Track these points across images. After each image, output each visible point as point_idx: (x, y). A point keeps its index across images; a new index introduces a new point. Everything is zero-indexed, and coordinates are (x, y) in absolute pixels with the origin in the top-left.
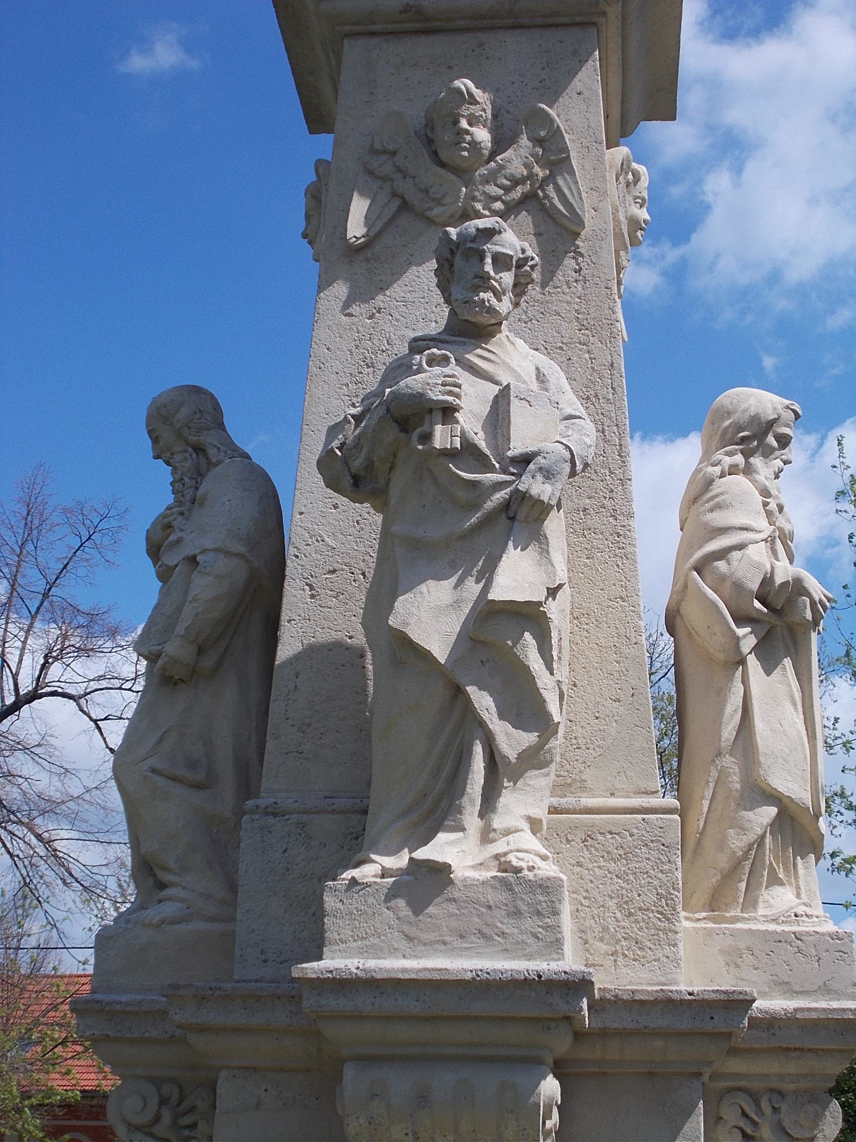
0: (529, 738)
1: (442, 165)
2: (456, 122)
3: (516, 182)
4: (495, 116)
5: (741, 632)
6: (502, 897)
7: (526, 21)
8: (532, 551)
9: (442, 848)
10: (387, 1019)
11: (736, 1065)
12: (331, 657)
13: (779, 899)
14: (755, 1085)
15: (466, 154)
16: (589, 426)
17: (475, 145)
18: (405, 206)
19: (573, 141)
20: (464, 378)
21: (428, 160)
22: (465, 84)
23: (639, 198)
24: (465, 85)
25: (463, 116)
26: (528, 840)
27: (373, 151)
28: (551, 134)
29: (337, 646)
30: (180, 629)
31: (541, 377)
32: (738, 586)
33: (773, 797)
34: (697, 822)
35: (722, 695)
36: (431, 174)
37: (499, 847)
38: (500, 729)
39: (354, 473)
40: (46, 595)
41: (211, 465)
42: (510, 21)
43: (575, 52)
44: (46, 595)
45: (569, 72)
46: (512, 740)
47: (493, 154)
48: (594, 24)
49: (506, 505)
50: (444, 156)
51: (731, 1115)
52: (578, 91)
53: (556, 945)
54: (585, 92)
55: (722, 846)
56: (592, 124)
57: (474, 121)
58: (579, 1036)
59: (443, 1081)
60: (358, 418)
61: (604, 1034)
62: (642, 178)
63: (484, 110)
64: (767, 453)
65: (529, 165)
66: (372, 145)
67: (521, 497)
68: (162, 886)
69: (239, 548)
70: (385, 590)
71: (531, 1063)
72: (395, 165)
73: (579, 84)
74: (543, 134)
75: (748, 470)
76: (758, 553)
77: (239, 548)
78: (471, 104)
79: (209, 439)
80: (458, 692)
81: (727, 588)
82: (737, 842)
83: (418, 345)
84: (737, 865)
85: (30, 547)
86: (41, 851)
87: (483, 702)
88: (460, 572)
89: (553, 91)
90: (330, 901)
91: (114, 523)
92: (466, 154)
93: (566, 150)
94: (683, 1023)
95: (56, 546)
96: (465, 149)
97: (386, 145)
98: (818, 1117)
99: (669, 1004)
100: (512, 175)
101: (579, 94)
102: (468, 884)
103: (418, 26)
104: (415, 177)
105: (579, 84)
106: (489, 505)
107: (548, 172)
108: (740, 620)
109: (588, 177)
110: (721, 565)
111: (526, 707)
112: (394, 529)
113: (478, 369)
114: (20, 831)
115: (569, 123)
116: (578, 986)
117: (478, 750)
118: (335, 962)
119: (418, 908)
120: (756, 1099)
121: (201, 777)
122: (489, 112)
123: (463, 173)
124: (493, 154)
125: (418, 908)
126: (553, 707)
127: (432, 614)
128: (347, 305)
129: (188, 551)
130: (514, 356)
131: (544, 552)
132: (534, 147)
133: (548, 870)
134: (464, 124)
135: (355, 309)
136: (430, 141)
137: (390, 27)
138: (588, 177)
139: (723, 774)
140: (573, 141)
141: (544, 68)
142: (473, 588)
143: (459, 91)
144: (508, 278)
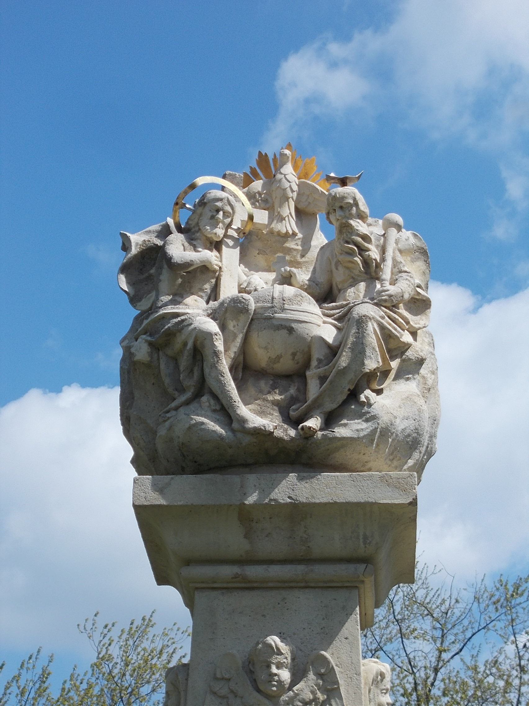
1: (259, 691)
2: (269, 667)
4: (293, 659)
7: (312, 585)
15: (275, 689)
17: (280, 682)
19: (342, 673)
21: (251, 688)
22: (274, 640)
23: (384, 690)
24: (274, 642)
25: (273, 663)
27: (216, 679)
28: (328, 671)
42: (302, 585)
43: (344, 608)
45: (340, 622)
48: (357, 587)
50: (262, 688)
52: (346, 637)
54: (350, 638)
56: (354, 662)
57: (280, 666)
62: (386, 676)
63: (286, 658)
65: (314, 692)
66: (215, 674)
72: (229, 688)
73: (346, 631)
74: (323, 671)
78: (278, 655)
88: (166, 327)
89: (328, 636)
92: (275, 689)
93: (337, 683)
96: (274, 686)
97: (224, 675)
100: (303, 699)
101: (346, 638)
103: (243, 585)
104: (242, 697)
105: (346, 631)
107: (325, 697)
109: (351, 699)
113: (218, 290)
115: (339, 660)
122: (289, 659)
132: (317, 679)
134: (274, 670)
137: (225, 585)
138: (351, 699)
140: (342, 673)
141: (323, 619)
143: (270, 646)
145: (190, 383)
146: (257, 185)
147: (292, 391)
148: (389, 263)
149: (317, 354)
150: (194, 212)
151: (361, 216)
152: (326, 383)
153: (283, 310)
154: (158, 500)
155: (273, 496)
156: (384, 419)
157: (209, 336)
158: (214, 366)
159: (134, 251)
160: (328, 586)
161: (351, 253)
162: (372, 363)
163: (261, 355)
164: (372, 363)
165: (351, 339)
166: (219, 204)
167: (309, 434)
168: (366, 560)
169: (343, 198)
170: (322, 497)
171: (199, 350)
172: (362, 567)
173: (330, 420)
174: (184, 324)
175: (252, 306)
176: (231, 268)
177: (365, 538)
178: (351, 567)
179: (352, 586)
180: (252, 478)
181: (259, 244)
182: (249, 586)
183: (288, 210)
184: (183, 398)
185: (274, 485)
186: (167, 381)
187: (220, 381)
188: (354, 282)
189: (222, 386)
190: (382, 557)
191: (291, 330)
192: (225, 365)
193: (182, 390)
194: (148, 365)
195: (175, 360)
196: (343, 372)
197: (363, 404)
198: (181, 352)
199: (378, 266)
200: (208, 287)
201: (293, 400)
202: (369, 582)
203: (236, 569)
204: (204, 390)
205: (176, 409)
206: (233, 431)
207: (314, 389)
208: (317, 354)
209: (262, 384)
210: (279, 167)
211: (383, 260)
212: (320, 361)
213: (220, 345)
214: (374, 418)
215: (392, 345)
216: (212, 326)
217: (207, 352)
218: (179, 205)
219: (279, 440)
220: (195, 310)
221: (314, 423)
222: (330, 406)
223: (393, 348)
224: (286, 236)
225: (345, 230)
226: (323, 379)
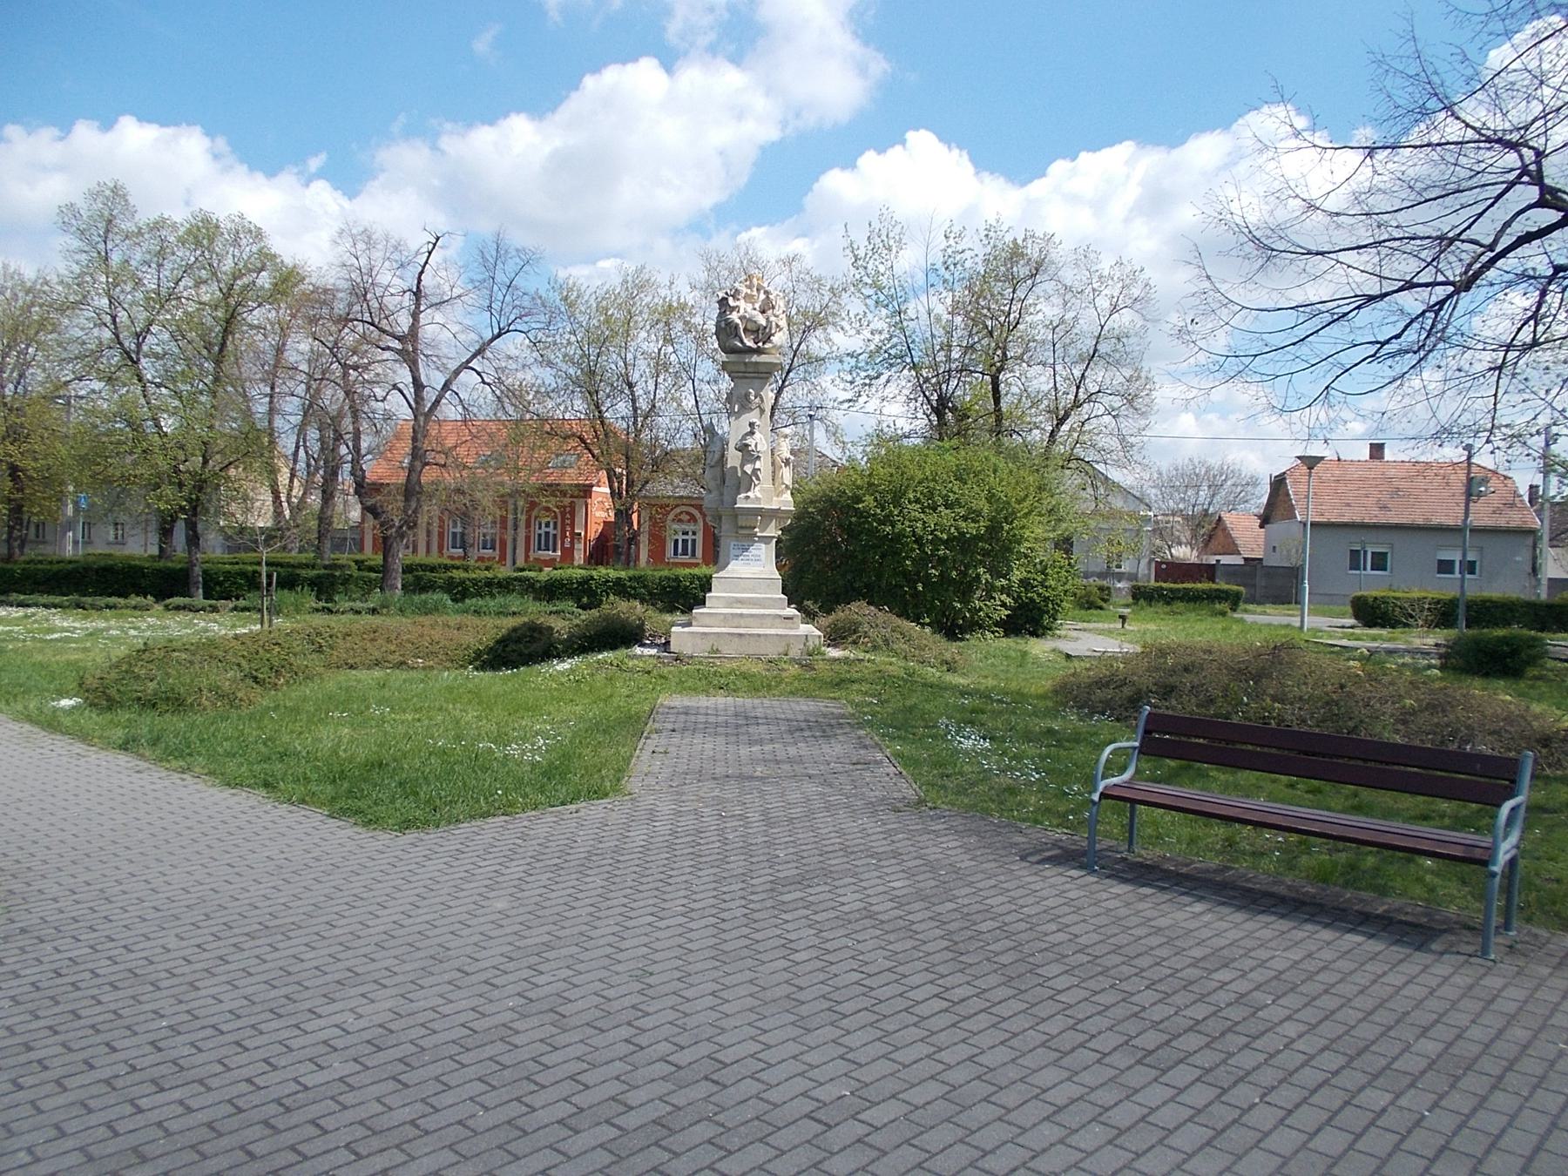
70: (742, 466)
127: (748, 469)
130: (758, 435)
171: (737, 326)
204: (737, 335)
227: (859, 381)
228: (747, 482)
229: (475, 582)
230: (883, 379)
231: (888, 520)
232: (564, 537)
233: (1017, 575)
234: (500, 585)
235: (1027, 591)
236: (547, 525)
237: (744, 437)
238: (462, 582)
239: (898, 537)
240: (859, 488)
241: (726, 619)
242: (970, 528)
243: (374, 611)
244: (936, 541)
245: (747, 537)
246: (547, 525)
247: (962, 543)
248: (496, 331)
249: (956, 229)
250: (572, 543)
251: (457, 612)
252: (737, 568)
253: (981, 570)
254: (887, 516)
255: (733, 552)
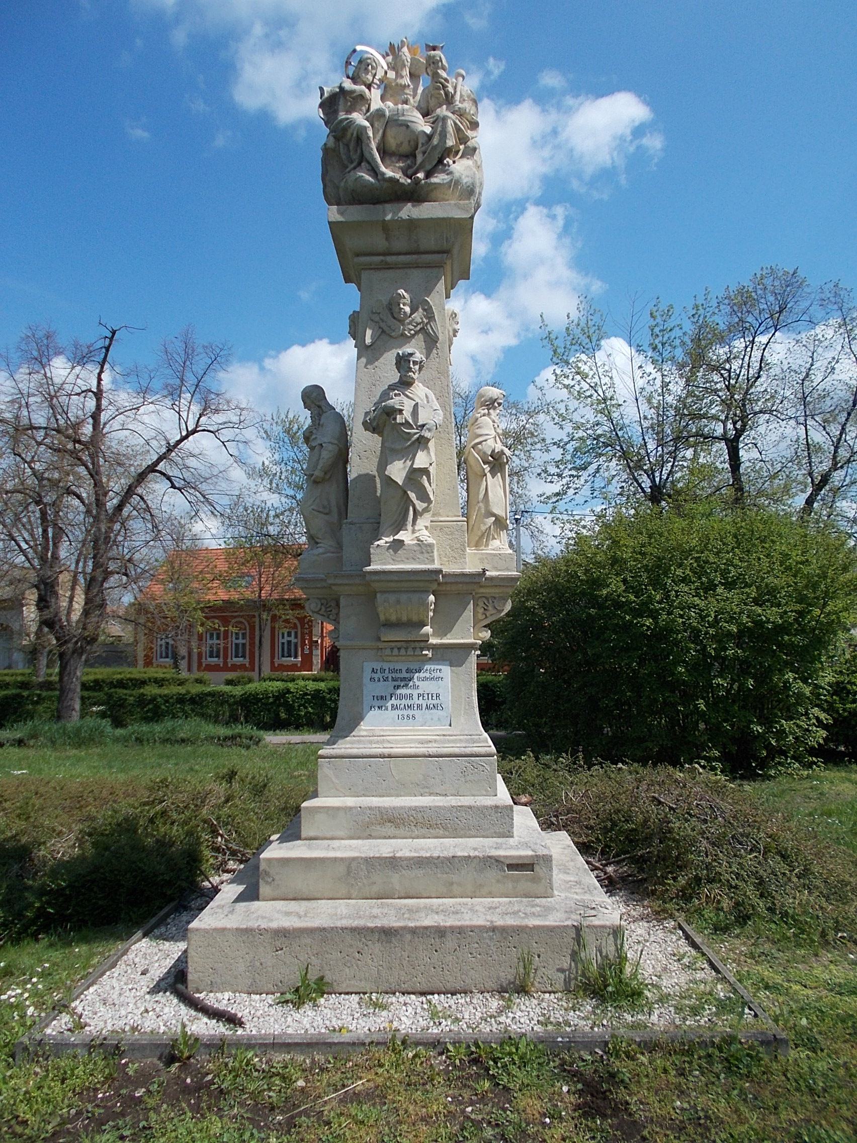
0: (425, 505)
1: (394, 318)
3: (418, 324)
5: (485, 467)
6: (419, 548)
8: (425, 452)
9: (401, 536)
10: (388, 581)
11: (482, 590)
12: (367, 479)
13: (496, 543)
14: (488, 596)
16: (440, 412)
18: (383, 332)
20: (405, 399)
26: (425, 532)
27: (373, 313)
29: (368, 475)
30: (319, 467)
31: (427, 397)
32: (485, 453)
33: (494, 515)
34: (472, 522)
35: (480, 485)
36: (391, 321)
37: (417, 535)
38: (416, 502)
39: (372, 426)
40: (197, 386)
41: (323, 412)
44: (197, 386)
46: (420, 506)
47: (411, 314)
49: (418, 439)
51: (481, 604)
53: (433, 560)
55: (479, 528)
58: (439, 584)
59: (404, 597)
60: (374, 411)
61: (446, 583)
64: (495, 408)
67: (421, 437)
68: (317, 543)
69: (336, 442)
70: (383, 465)
71: (427, 592)
75: (489, 414)
76: (491, 442)
77: (336, 442)
79: (322, 403)
80: (405, 492)
81: (481, 454)
82: (483, 528)
83: (392, 388)
84: (483, 535)
85: (188, 363)
86: (202, 499)
87: (412, 496)
89: (429, 292)
90: (372, 551)
91: (225, 352)
94: (467, 580)
95: (200, 363)
98: (504, 605)
99: (463, 575)
102: (409, 545)
106: (413, 439)
108: (485, 463)
110: (479, 446)
111: (424, 496)
112: (386, 444)
114: (192, 491)
116: (440, 571)
117: (411, 508)
118: (373, 567)
119: (396, 551)
120: (487, 599)
121: (327, 511)
123: (401, 321)
124: (411, 314)
125: (396, 551)
126: (431, 496)
127: (397, 471)
128: (365, 367)
129: (319, 442)
130: (419, 390)
131: (429, 452)
133: (431, 540)
134: (402, 306)
135: (368, 367)
136: (391, 309)
139: (480, 508)
142: (409, 463)
144: (417, 367)
145: (355, 157)
146: (390, 58)
147: (409, 162)
148: (458, 93)
149: (422, 140)
150: (356, 67)
151: (444, 68)
152: (428, 156)
153: (403, 115)
154: (340, 218)
155: (400, 215)
156: (457, 175)
157: (365, 128)
158: (368, 145)
159: (326, 95)
160: (429, 266)
161: (439, 88)
162: (450, 143)
163: (392, 143)
164: (450, 143)
165: (439, 129)
166: (369, 61)
167: (418, 181)
168: (447, 252)
169: (434, 57)
170: (425, 216)
171: (360, 138)
172: (445, 255)
173: (428, 175)
174: (351, 122)
175: (387, 114)
176: (375, 98)
177: (447, 239)
178: (440, 255)
179: (440, 266)
180: (388, 206)
181: (390, 92)
182: (388, 267)
183: (406, 72)
184: (352, 166)
185: (400, 210)
186: (344, 157)
187: (371, 153)
188: (440, 106)
189: (372, 155)
190: (455, 251)
191: (408, 126)
192: (374, 146)
193: (352, 162)
194: (334, 150)
195: (347, 145)
196: (435, 147)
197: (445, 165)
198: (350, 140)
199: (453, 96)
200: (364, 109)
201: (410, 167)
202: (449, 262)
203: (381, 258)
204: (364, 160)
205: (349, 172)
206: (378, 180)
207: (420, 158)
208: (422, 140)
209: (393, 159)
210: (399, 49)
211: (455, 92)
212: (423, 144)
213: (370, 134)
214: (451, 173)
215: (461, 136)
216: (367, 124)
217: (364, 138)
218: (348, 63)
219: (403, 184)
220: (358, 118)
221: (421, 175)
222: (429, 167)
223: (463, 139)
224: (405, 86)
225: (436, 76)
226: (424, 153)
227: (566, 473)
228: (395, 505)
229: (167, 699)
230: (592, 469)
231: (645, 609)
232: (303, 644)
233: (827, 678)
234: (193, 701)
235: (843, 701)
236: (289, 634)
237: (385, 395)
238: (154, 699)
239: (663, 634)
240: (599, 565)
241: (356, 877)
242: (771, 615)
243: (20, 743)
244: (722, 638)
245: (404, 654)
246: (289, 634)
247: (758, 636)
248: (184, 433)
249: (663, 307)
250: (311, 649)
251: (117, 740)
252: (381, 730)
253: (790, 676)
254: (644, 604)
255: (371, 689)
